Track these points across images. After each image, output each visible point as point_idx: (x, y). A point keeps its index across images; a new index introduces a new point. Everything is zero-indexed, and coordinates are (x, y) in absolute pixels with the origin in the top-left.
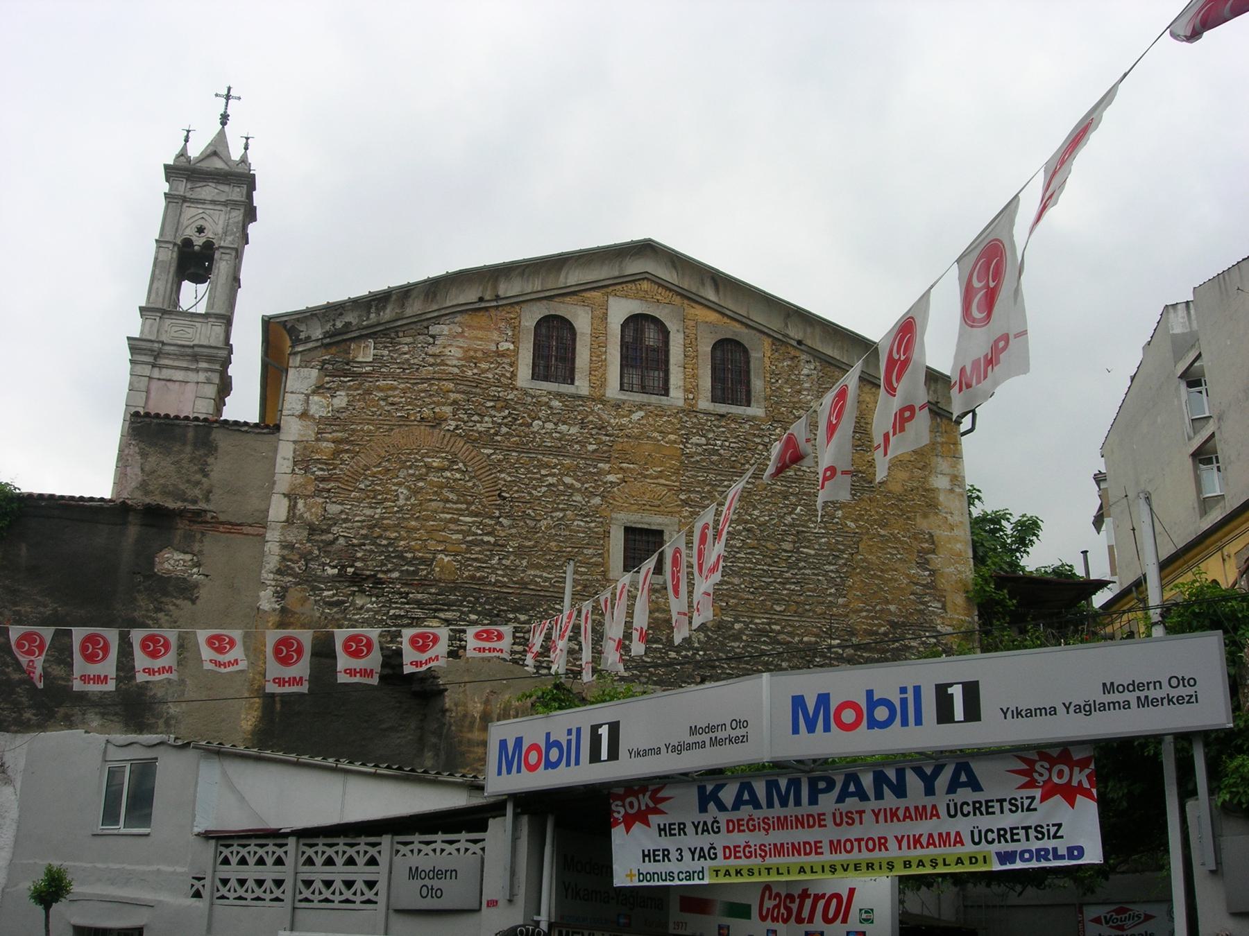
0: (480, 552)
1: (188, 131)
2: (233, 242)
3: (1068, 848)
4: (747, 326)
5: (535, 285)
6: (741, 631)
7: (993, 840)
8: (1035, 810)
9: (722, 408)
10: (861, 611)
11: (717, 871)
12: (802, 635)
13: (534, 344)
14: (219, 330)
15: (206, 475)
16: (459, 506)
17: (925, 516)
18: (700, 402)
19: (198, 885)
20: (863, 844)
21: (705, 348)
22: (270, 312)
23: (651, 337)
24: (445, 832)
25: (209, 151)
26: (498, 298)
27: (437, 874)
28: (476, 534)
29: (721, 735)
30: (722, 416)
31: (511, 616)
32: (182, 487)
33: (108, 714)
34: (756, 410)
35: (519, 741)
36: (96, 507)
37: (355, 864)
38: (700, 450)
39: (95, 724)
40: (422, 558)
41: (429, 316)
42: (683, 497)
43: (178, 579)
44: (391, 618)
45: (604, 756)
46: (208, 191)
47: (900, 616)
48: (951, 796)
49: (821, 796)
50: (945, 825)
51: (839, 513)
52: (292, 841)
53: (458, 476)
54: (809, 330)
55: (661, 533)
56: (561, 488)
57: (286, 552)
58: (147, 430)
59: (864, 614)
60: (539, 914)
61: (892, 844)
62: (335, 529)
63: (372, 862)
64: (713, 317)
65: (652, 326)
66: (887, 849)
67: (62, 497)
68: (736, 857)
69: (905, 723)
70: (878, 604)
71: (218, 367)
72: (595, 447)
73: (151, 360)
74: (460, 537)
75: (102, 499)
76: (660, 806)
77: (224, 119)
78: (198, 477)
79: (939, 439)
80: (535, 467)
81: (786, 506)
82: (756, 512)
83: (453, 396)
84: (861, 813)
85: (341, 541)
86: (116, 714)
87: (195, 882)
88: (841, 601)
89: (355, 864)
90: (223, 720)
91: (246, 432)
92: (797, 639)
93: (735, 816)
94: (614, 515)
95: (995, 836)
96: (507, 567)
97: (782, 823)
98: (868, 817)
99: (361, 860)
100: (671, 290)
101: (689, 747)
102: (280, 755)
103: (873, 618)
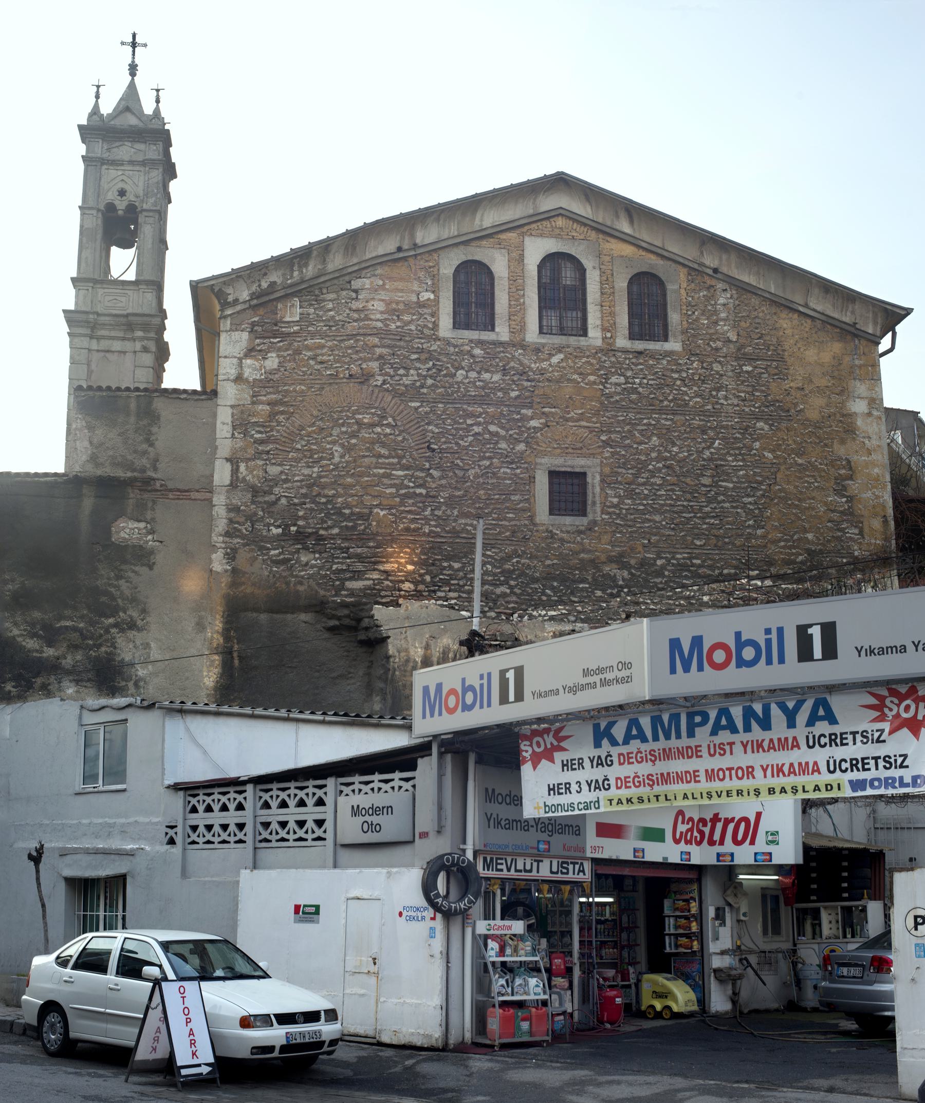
0: (413, 504)
2: (155, 204)
3: (913, 777)
4: (663, 257)
5: (451, 230)
6: (663, 567)
7: (847, 769)
8: (884, 741)
9: (640, 345)
10: (780, 540)
11: (611, 801)
12: (722, 568)
13: (454, 292)
14: (150, 297)
15: (152, 445)
16: (391, 460)
17: (843, 442)
18: (617, 340)
19: (171, 832)
20: (733, 772)
21: (622, 284)
22: (196, 278)
23: (568, 276)
24: (381, 773)
26: (415, 246)
27: (376, 810)
28: (409, 487)
29: (609, 676)
30: (640, 353)
31: (445, 564)
32: (129, 457)
33: (81, 680)
34: (674, 345)
35: (439, 687)
36: (50, 482)
37: (306, 805)
38: (619, 389)
39: (70, 691)
40: (359, 513)
41: (350, 270)
42: (604, 438)
43: (134, 546)
44: (334, 572)
45: (512, 698)
46: (125, 151)
47: (818, 544)
48: (810, 729)
49: (697, 730)
50: (803, 755)
51: (757, 445)
52: (249, 788)
53: (388, 431)
54: (724, 257)
55: (584, 474)
56: (487, 436)
57: (232, 515)
58: (93, 402)
59: (782, 544)
60: (464, 843)
61: (758, 773)
62: (276, 490)
63: (320, 802)
64: (628, 250)
65: (569, 265)
66: (754, 777)
67: (18, 474)
68: (626, 787)
69: (769, 662)
70: (796, 533)
71: (152, 335)
72: (517, 393)
73: (88, 332)
74: (394, 490)
75: (56, 474)
76: (562, 744)
77: (133, 69)
78: (145, 446)
79: (857, 362)
80: (460, 417)
81: (705, 441)
82: (675, 449)
83: (378, 351)
84: (731, 744)
85: (283, 501)
86: (89, 680)
87: (169, 830)
88: (759, 532)
89: (306, 805)
90: (187, 678)
91: (186, 399)
92: (717, 572)
93: (624, 750)
94: (538, 460)
95: (848, 765)
96: (439, 517)
97: (667, 754)
98: (738, 748)
99: (310, 802)
100: (585, 225)
101: (583, 687)
102: (236, 709)
103: (790, 548)
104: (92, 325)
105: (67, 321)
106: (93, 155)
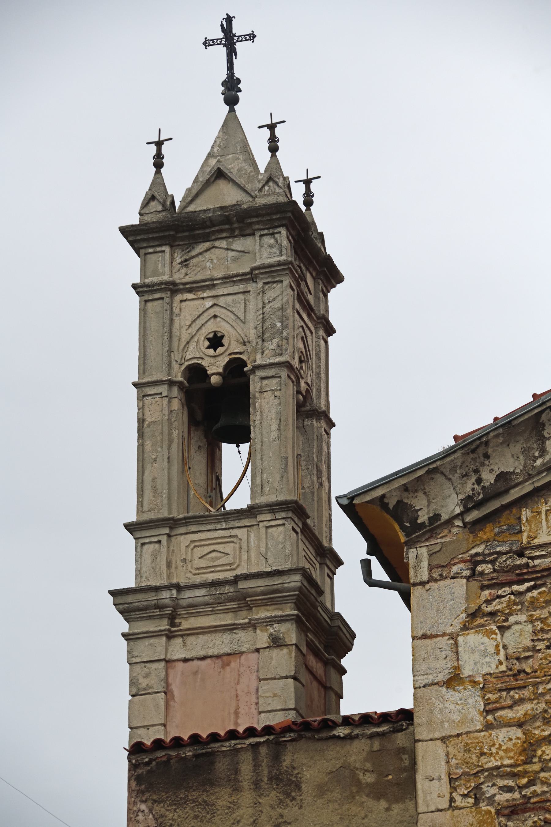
1: (159, 144)
25: (149, 197)
46: (216, 259)
77: (231, 90)
91: (350, 738)
104: (168, 611)
105: (121, 612)
106: (155, 280)
